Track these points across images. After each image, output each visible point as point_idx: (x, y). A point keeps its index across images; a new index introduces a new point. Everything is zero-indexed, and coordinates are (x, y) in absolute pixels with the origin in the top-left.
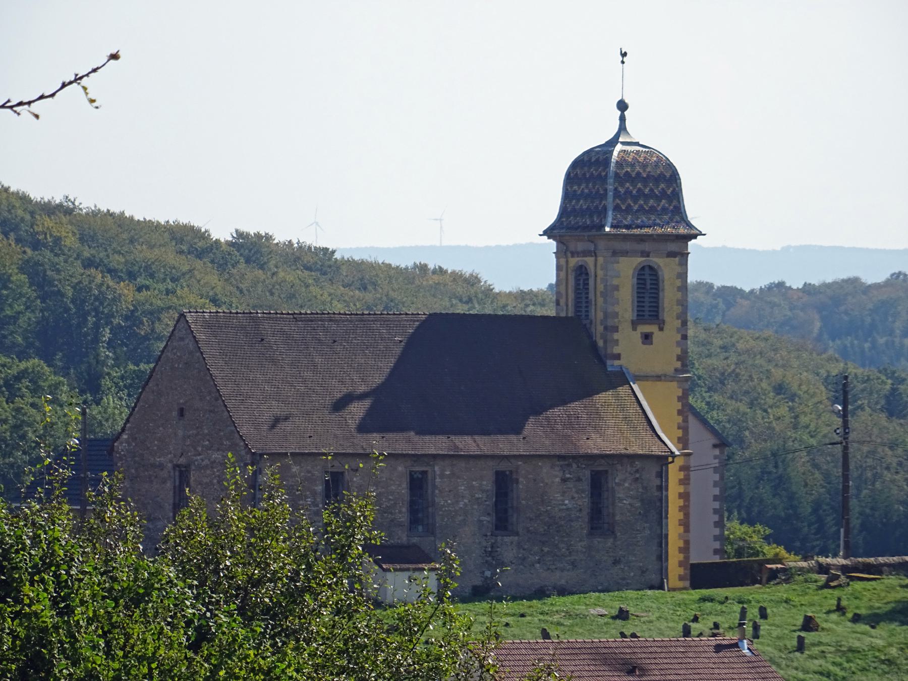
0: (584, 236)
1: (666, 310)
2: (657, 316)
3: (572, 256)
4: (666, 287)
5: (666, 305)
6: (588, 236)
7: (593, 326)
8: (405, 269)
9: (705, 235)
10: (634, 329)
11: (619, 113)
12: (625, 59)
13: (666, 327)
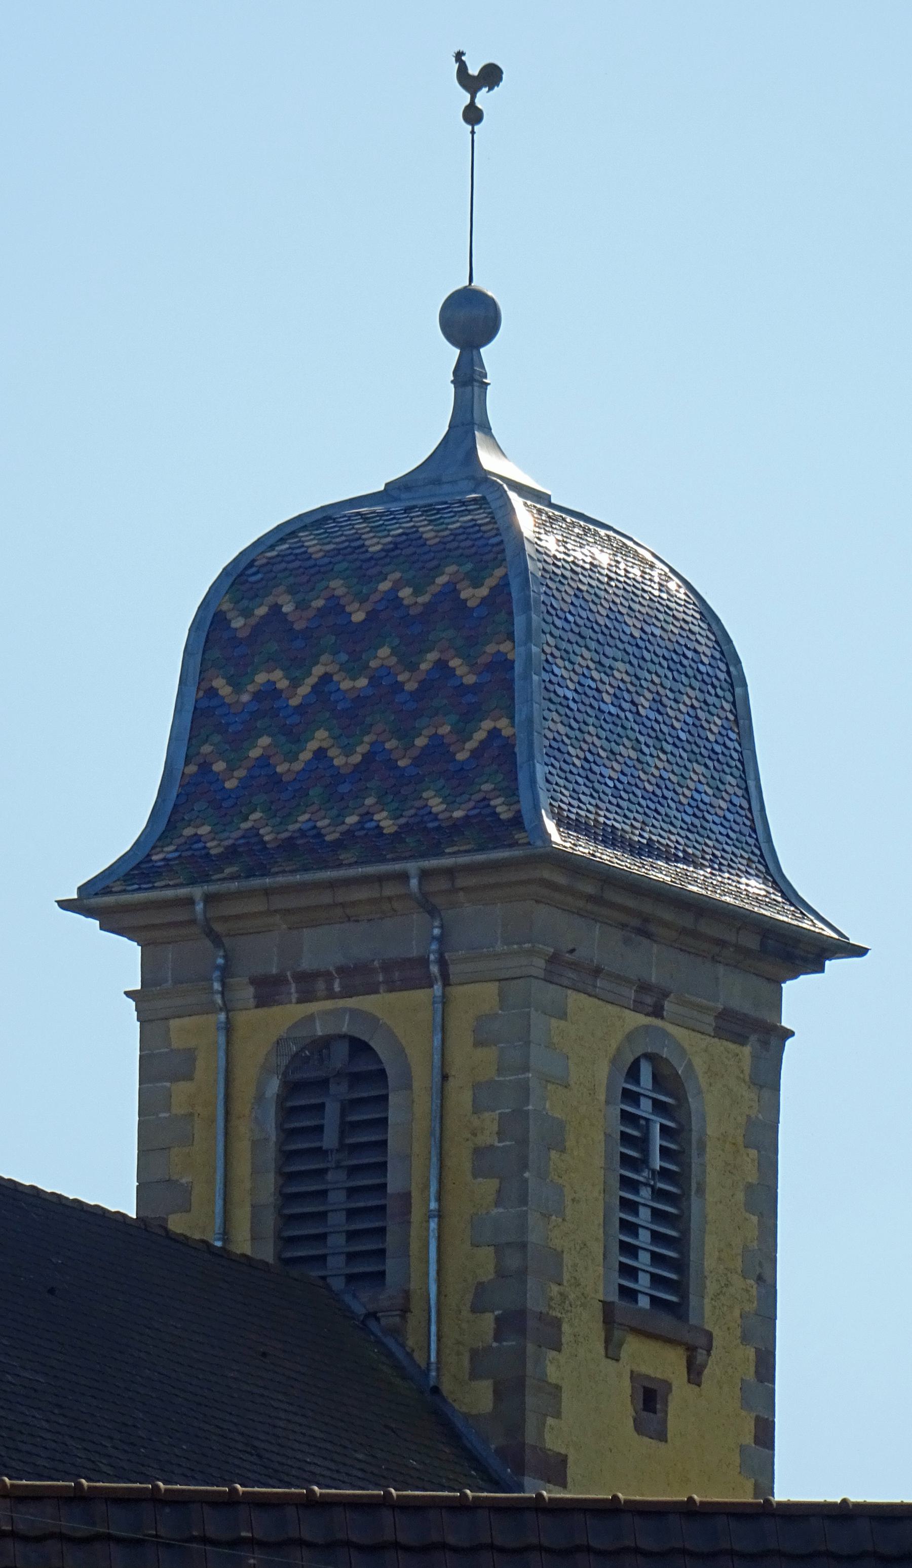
0: (404, 877)
1: (711, 1287)
2: (678, 1311)
3: (262, 1002)
4: (712, 1178)
5: (710, 1263)
6: (425, 875)
7: (414, 1320)
8: (510, 661)
9: (860, 952)
10: (612, 1351)
11: (454, 353)
12: (483, 98)
13: (713, 1369)
